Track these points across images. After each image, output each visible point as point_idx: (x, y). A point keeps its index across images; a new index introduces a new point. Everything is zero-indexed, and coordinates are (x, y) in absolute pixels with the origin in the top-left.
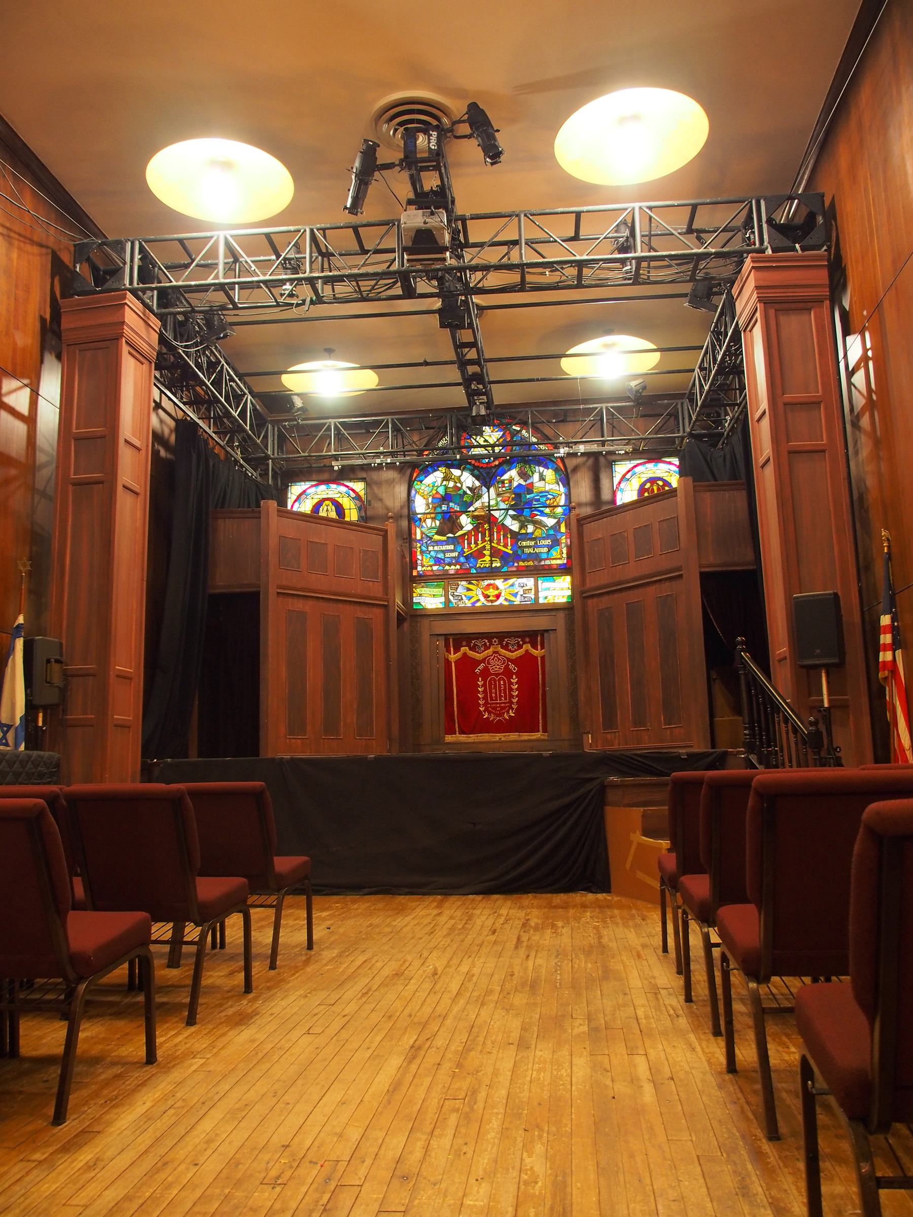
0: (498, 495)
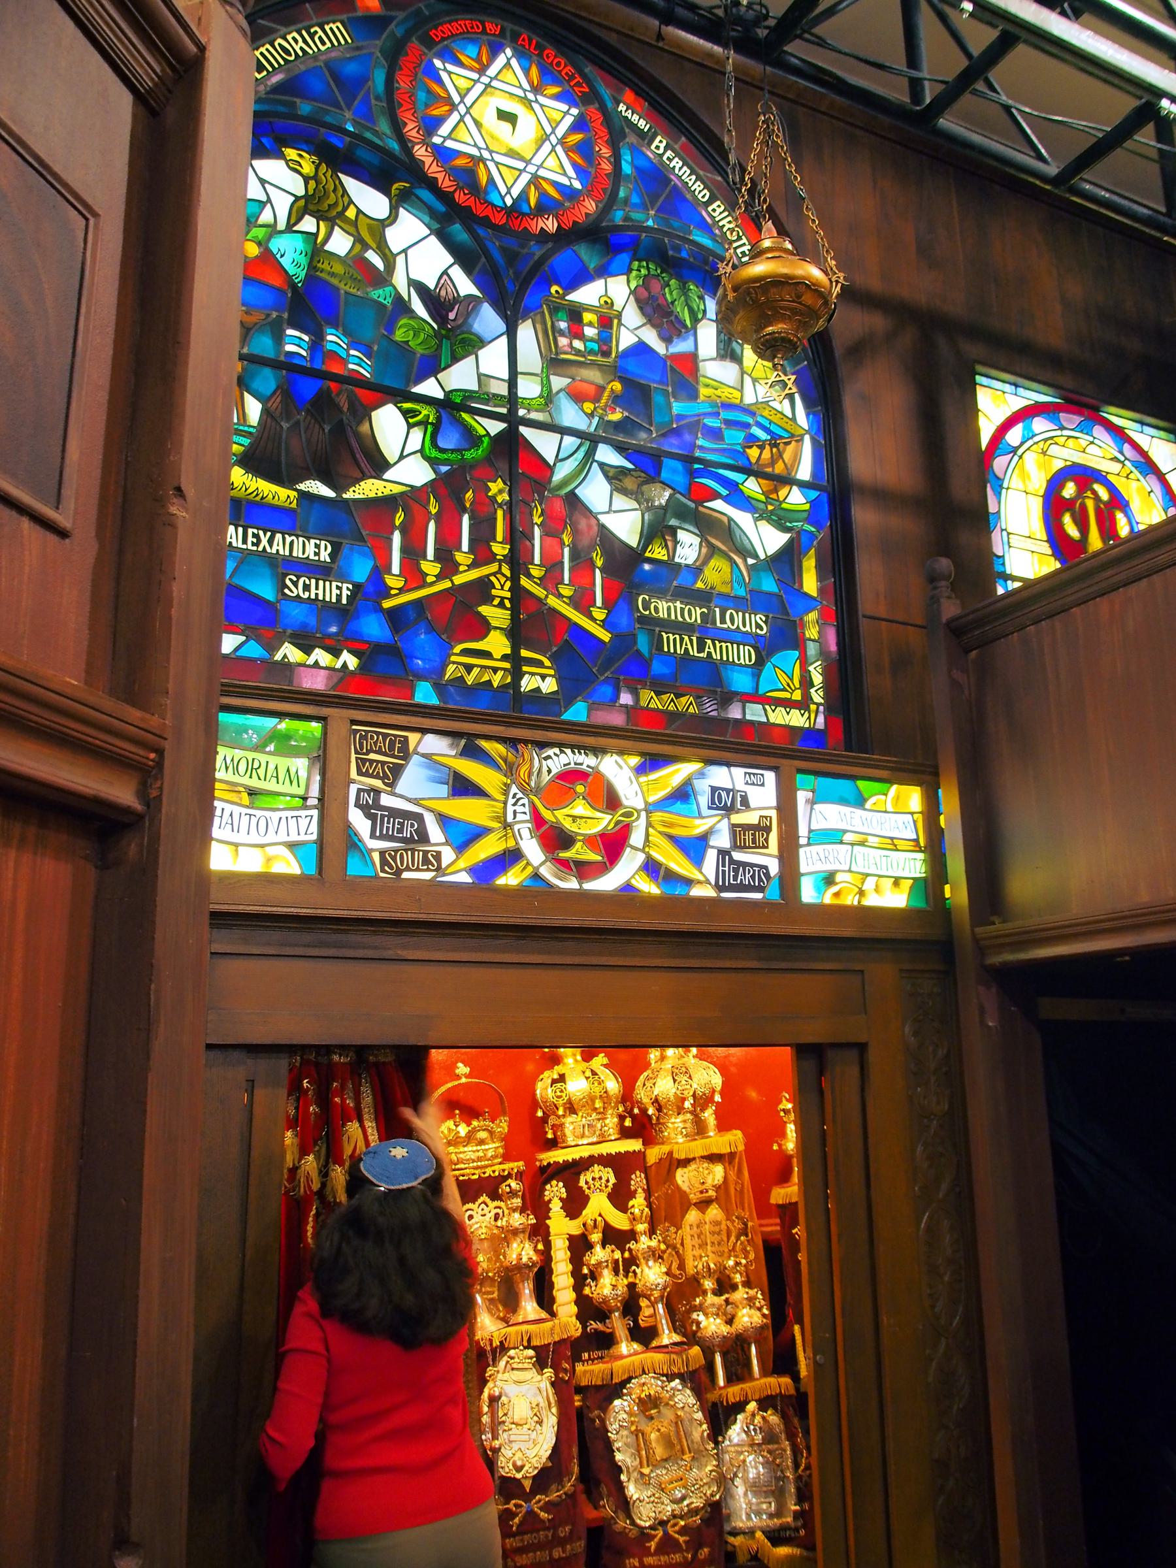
0: (554, 363)
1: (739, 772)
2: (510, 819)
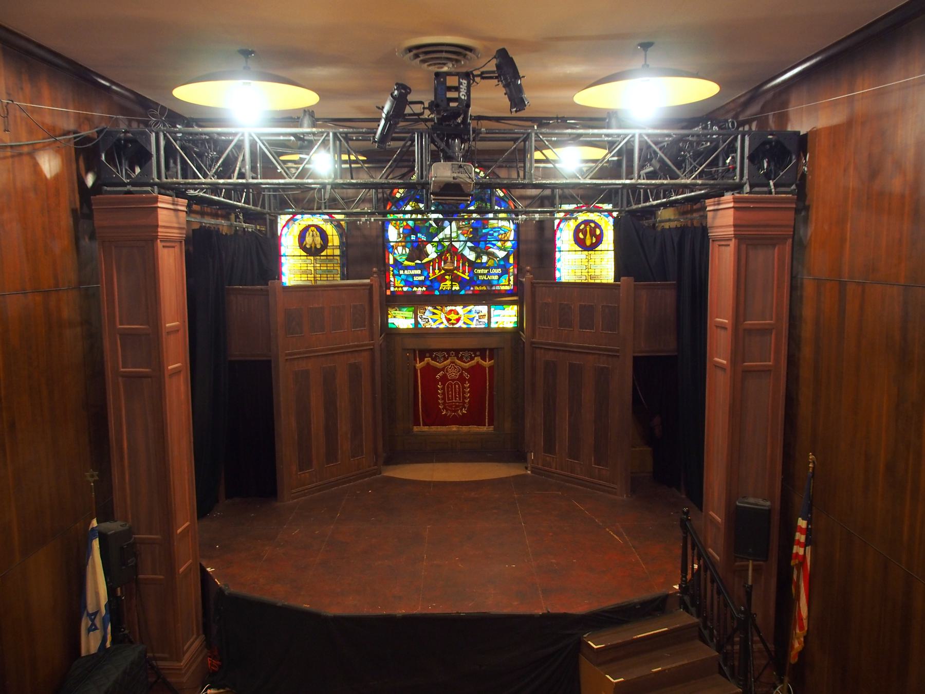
0: (459, 228)
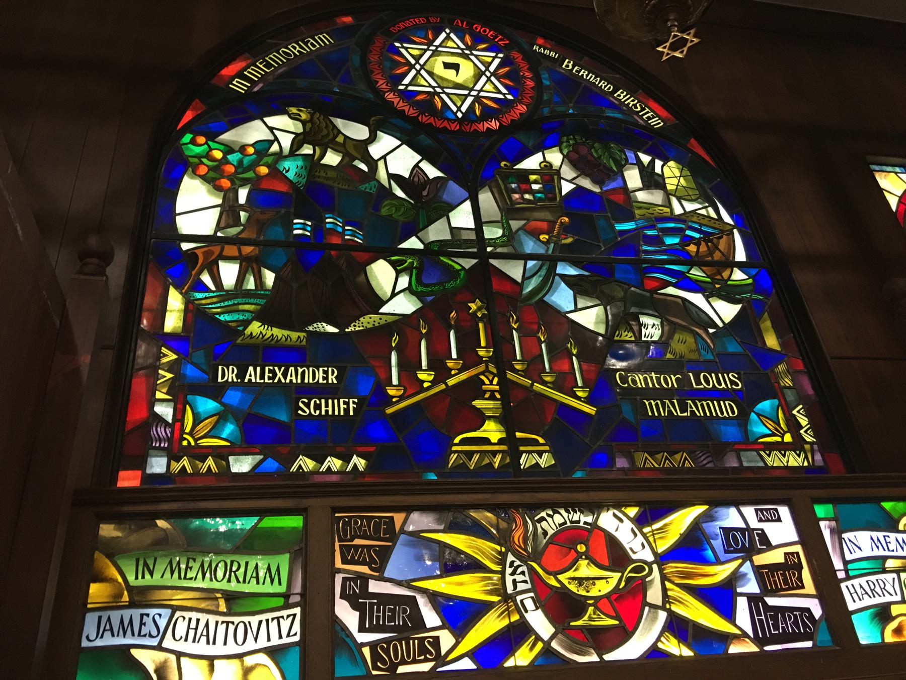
0: (509, 211)
1: (749, 511)
2: (510, 589)
